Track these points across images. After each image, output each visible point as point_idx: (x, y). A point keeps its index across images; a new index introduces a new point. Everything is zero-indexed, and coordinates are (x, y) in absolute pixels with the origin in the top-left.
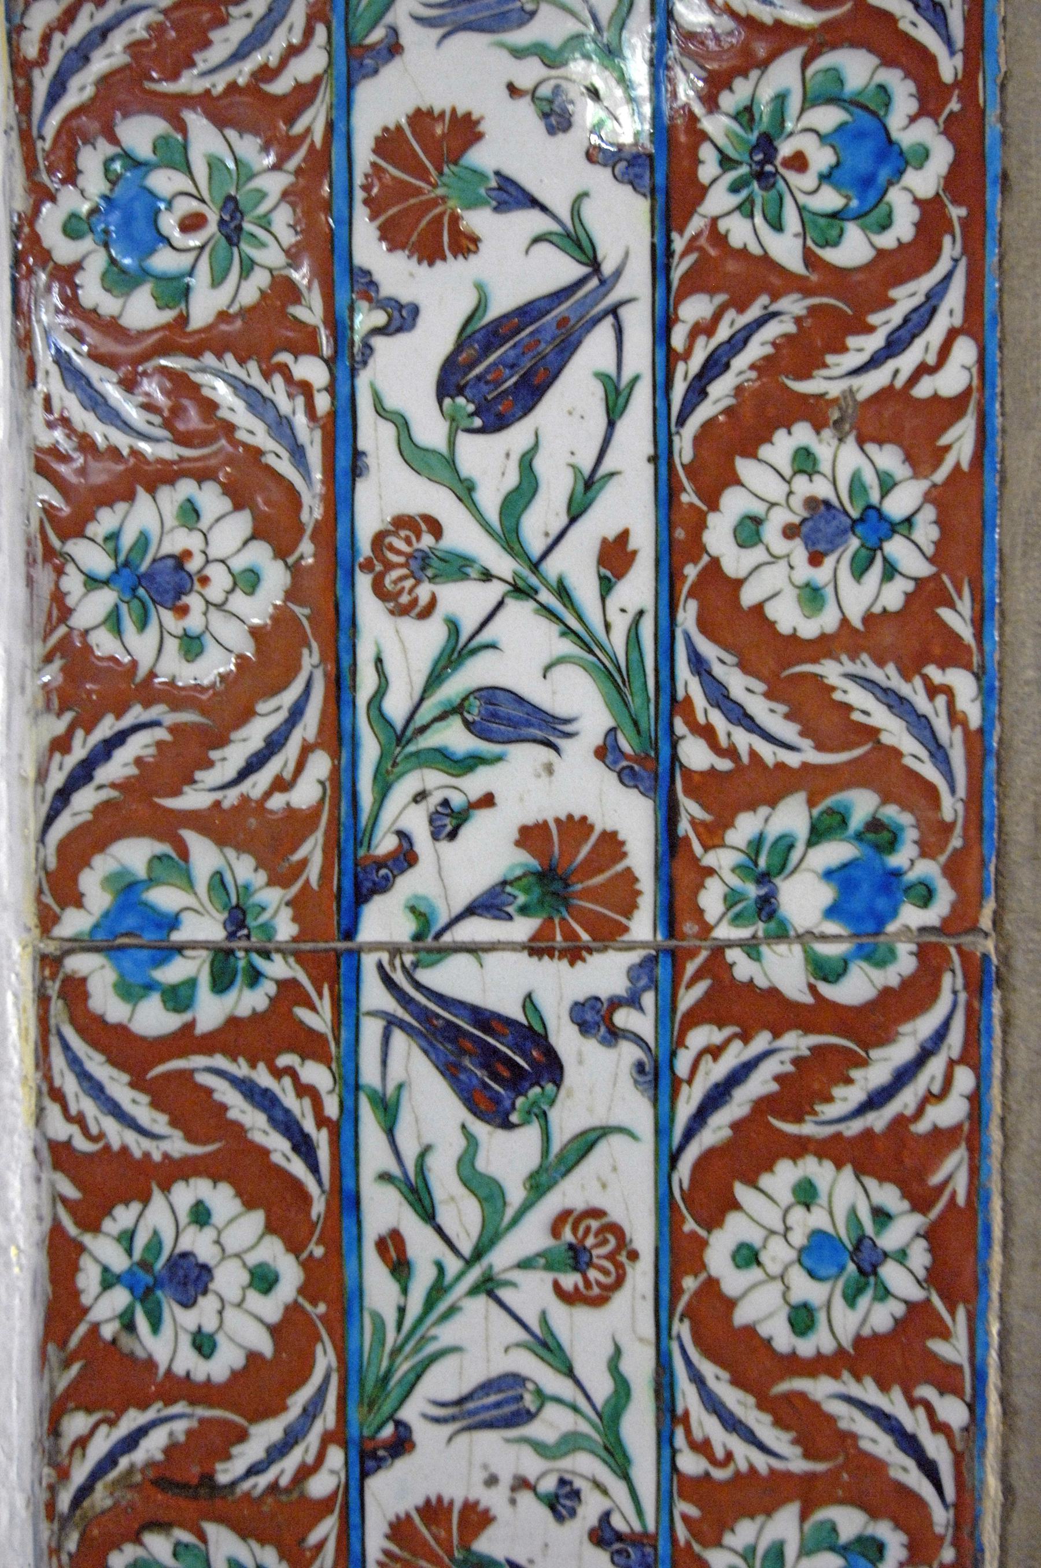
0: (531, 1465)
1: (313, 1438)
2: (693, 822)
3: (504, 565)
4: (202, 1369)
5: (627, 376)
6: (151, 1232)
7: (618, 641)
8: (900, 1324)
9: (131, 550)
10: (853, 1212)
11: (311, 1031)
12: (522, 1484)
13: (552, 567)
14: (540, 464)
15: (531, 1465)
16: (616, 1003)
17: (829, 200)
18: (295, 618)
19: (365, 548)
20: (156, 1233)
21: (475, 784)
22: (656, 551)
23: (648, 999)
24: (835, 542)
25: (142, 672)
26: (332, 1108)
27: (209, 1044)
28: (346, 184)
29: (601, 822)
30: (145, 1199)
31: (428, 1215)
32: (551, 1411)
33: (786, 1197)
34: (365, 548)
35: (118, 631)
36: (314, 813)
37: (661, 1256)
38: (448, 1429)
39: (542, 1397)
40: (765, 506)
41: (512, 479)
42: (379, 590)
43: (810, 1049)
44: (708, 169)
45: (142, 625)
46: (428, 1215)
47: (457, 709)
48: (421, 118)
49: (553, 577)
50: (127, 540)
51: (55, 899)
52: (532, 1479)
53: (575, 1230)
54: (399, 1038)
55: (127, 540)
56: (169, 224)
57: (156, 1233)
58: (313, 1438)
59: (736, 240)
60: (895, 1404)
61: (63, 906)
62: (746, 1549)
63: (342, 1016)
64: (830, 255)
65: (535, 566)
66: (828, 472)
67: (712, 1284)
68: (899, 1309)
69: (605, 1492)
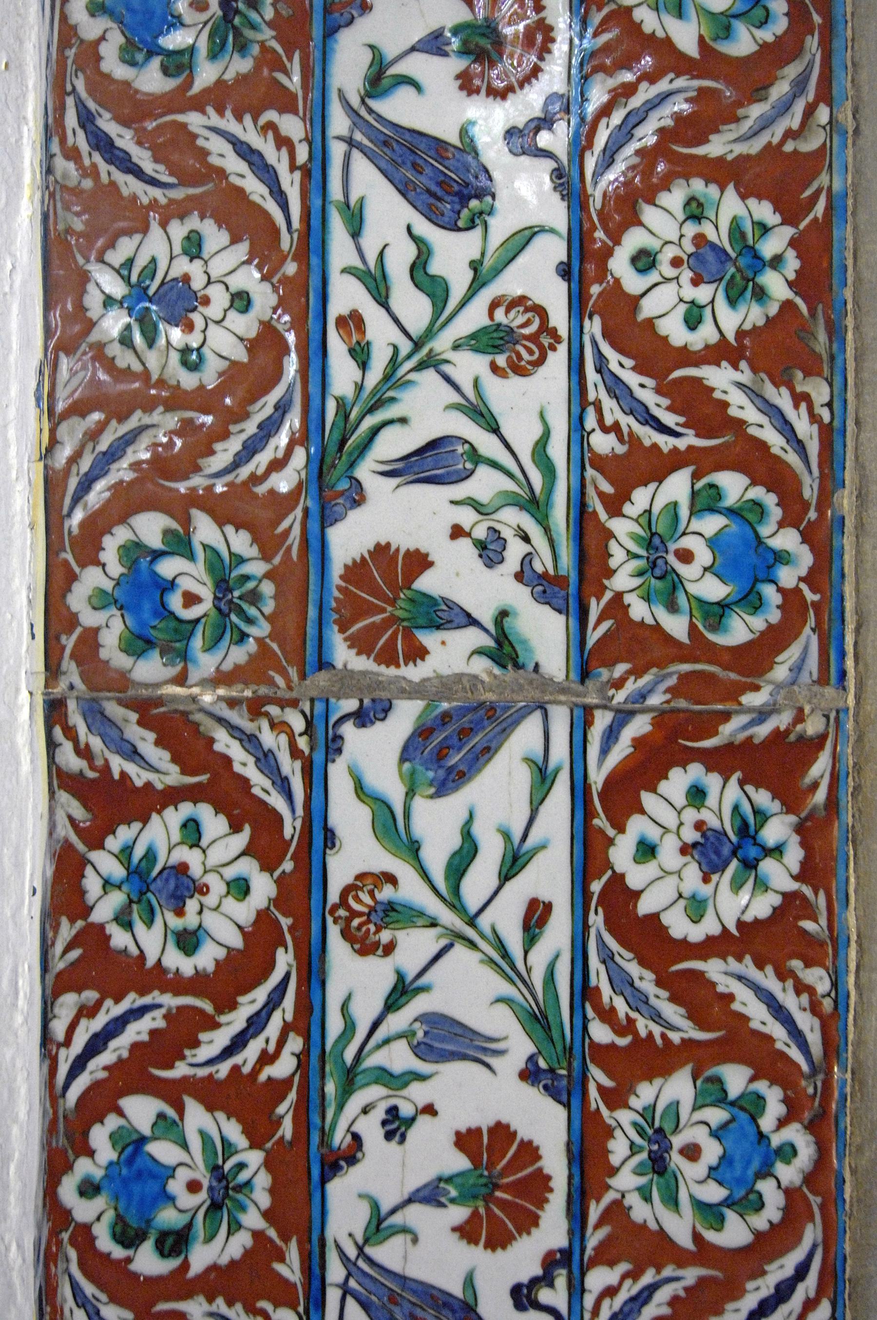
0: (466, 517)
1: (283, 439)
2: (601, 1088)
3: (447, 917)
4: (188, 381)
5: (552, 765)
6: (148, 259)
7: (537, 979)
8: (778, 912)
9: (141, 860)
10: (736, 808)
11: (286, 1282)
12: (457, 532)
13: (484, 922)
14: (477, 830)
15: (466, 517)
16: (535, 1282)
17: (714, 1193)
18: (277, 923)
19: (333, 896)
20: (153, 260)
21: (419, 1093)
22: (572, 932)
23: (561, 1282)
24: (721, 868)
25: (150, 962)
26: (302, 154)
27: (198, 105)
28: (321, 872)
29: (524, 1132)
30: (145, 820)
31: (383, 300)
32: (483, 472)
33: (680, 799)
34: (333, 896)
35: (128, 926)
36: (288, 1082)
37: (576, 813)
38: (395, 481)
39: (475, 457)
40: (660, 831)
41: (456, 842)
42: (346, 934)
43: (708, 141)
44: (617, 556)
45: (149, 923)
46: (383, 300)
47: (406, 1035)
48: (381, 551)
49: (487, 931)
50: (139, 852)
51: (74, 557)
52: (467, 529)
53: (507, 312)
54: (357, 157)
55: (139, 852)
56: (176, 1187)
57: (153, 260)
58: (283, 439)
59: (647, 28)
60: (769, 980)
61: (83, 565)
62: (645, 1109)
63: (310, 386)
64: (710, 1236)
65: (472, 922)
66: (715, 807)
67: (618, 879)
68: (777, 900)
69: (526, 539)
